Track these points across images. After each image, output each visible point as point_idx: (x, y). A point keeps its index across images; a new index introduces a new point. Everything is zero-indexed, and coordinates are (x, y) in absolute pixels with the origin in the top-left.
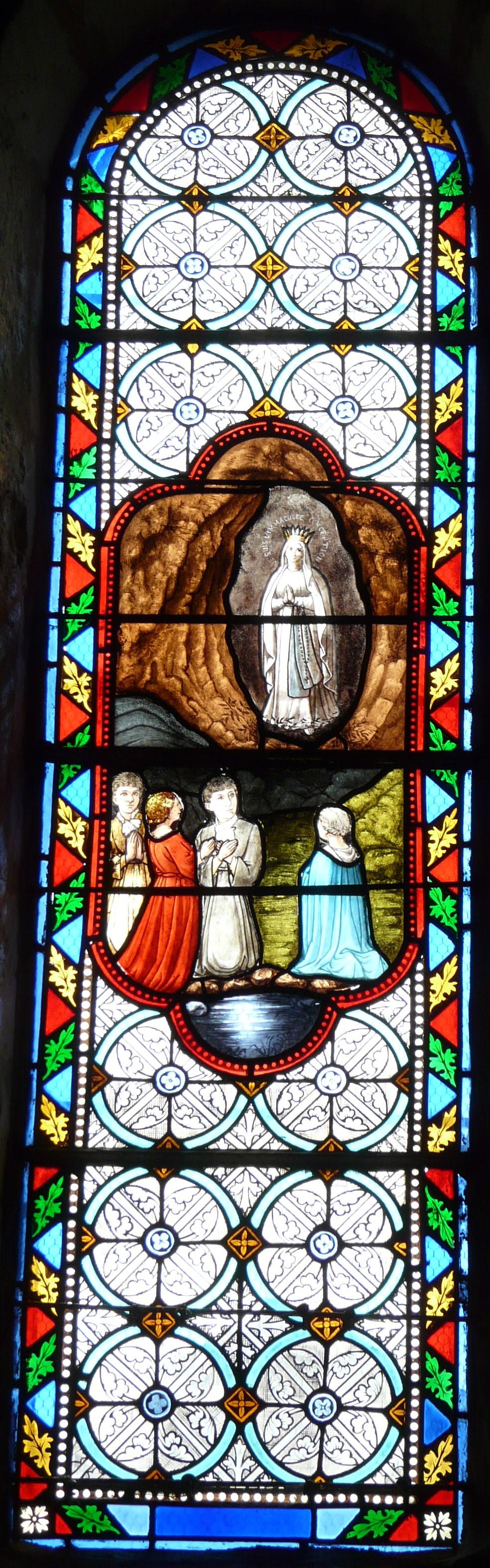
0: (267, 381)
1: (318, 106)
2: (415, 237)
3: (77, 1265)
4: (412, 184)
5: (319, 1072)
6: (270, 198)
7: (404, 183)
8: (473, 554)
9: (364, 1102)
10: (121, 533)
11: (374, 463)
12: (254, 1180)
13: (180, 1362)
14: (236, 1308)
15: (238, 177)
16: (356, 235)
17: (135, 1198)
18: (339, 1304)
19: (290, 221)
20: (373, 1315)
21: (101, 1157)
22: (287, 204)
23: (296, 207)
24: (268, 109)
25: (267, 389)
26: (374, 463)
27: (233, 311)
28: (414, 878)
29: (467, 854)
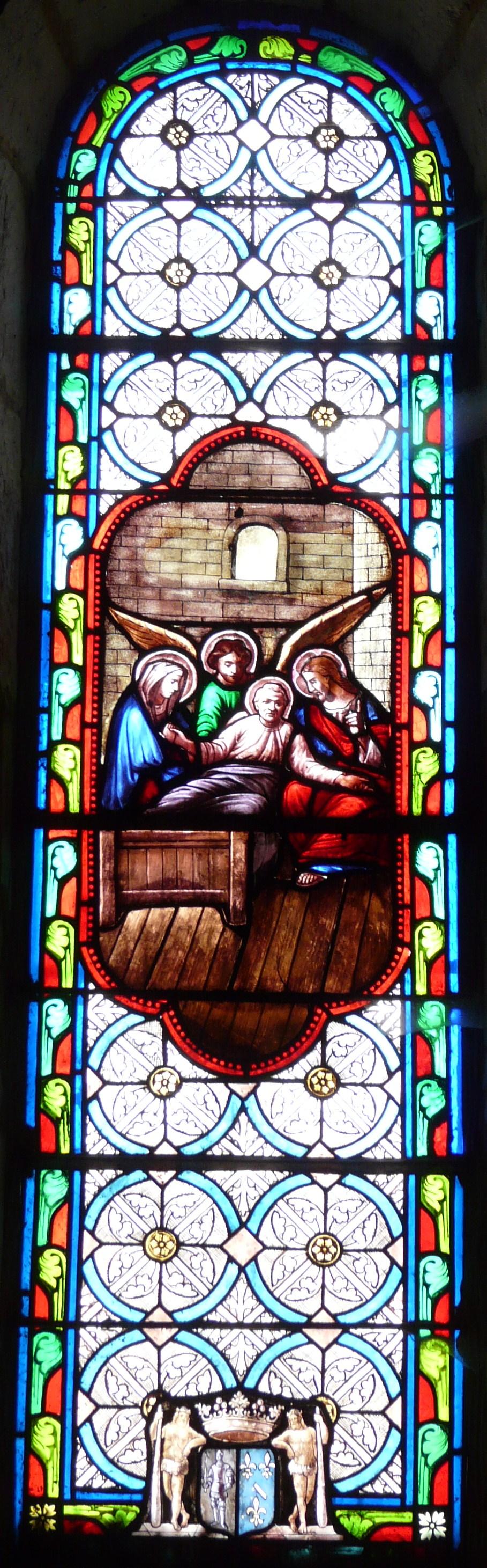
0: (242, 1284)
1: (296, 104)
2: (398, 1212)
3: (99, 439)
4: (393, 188)
5: (310, 1240)
6: (240, 1325)
7: (384, 1475)
8: (456, 612)
9: (355, 1273)
10: (111, 539)
11: (356, 1308)
12: (252, 1184)
13: (185, 1207)
14: (248, 194)
15: (219, 318)
16: (336, 384)
17: (134, 1204)
18: (340, 188)
19: (262, 1352)
20: (367, 199)
21: (116, 344)
22: (259, 1332)
23: (268, 1335)
24: (234, 1372)
25: (241, 1379)
26: (356, 1308)
27: (216, 321)
28: (402, 899)
29: (457, 1461)
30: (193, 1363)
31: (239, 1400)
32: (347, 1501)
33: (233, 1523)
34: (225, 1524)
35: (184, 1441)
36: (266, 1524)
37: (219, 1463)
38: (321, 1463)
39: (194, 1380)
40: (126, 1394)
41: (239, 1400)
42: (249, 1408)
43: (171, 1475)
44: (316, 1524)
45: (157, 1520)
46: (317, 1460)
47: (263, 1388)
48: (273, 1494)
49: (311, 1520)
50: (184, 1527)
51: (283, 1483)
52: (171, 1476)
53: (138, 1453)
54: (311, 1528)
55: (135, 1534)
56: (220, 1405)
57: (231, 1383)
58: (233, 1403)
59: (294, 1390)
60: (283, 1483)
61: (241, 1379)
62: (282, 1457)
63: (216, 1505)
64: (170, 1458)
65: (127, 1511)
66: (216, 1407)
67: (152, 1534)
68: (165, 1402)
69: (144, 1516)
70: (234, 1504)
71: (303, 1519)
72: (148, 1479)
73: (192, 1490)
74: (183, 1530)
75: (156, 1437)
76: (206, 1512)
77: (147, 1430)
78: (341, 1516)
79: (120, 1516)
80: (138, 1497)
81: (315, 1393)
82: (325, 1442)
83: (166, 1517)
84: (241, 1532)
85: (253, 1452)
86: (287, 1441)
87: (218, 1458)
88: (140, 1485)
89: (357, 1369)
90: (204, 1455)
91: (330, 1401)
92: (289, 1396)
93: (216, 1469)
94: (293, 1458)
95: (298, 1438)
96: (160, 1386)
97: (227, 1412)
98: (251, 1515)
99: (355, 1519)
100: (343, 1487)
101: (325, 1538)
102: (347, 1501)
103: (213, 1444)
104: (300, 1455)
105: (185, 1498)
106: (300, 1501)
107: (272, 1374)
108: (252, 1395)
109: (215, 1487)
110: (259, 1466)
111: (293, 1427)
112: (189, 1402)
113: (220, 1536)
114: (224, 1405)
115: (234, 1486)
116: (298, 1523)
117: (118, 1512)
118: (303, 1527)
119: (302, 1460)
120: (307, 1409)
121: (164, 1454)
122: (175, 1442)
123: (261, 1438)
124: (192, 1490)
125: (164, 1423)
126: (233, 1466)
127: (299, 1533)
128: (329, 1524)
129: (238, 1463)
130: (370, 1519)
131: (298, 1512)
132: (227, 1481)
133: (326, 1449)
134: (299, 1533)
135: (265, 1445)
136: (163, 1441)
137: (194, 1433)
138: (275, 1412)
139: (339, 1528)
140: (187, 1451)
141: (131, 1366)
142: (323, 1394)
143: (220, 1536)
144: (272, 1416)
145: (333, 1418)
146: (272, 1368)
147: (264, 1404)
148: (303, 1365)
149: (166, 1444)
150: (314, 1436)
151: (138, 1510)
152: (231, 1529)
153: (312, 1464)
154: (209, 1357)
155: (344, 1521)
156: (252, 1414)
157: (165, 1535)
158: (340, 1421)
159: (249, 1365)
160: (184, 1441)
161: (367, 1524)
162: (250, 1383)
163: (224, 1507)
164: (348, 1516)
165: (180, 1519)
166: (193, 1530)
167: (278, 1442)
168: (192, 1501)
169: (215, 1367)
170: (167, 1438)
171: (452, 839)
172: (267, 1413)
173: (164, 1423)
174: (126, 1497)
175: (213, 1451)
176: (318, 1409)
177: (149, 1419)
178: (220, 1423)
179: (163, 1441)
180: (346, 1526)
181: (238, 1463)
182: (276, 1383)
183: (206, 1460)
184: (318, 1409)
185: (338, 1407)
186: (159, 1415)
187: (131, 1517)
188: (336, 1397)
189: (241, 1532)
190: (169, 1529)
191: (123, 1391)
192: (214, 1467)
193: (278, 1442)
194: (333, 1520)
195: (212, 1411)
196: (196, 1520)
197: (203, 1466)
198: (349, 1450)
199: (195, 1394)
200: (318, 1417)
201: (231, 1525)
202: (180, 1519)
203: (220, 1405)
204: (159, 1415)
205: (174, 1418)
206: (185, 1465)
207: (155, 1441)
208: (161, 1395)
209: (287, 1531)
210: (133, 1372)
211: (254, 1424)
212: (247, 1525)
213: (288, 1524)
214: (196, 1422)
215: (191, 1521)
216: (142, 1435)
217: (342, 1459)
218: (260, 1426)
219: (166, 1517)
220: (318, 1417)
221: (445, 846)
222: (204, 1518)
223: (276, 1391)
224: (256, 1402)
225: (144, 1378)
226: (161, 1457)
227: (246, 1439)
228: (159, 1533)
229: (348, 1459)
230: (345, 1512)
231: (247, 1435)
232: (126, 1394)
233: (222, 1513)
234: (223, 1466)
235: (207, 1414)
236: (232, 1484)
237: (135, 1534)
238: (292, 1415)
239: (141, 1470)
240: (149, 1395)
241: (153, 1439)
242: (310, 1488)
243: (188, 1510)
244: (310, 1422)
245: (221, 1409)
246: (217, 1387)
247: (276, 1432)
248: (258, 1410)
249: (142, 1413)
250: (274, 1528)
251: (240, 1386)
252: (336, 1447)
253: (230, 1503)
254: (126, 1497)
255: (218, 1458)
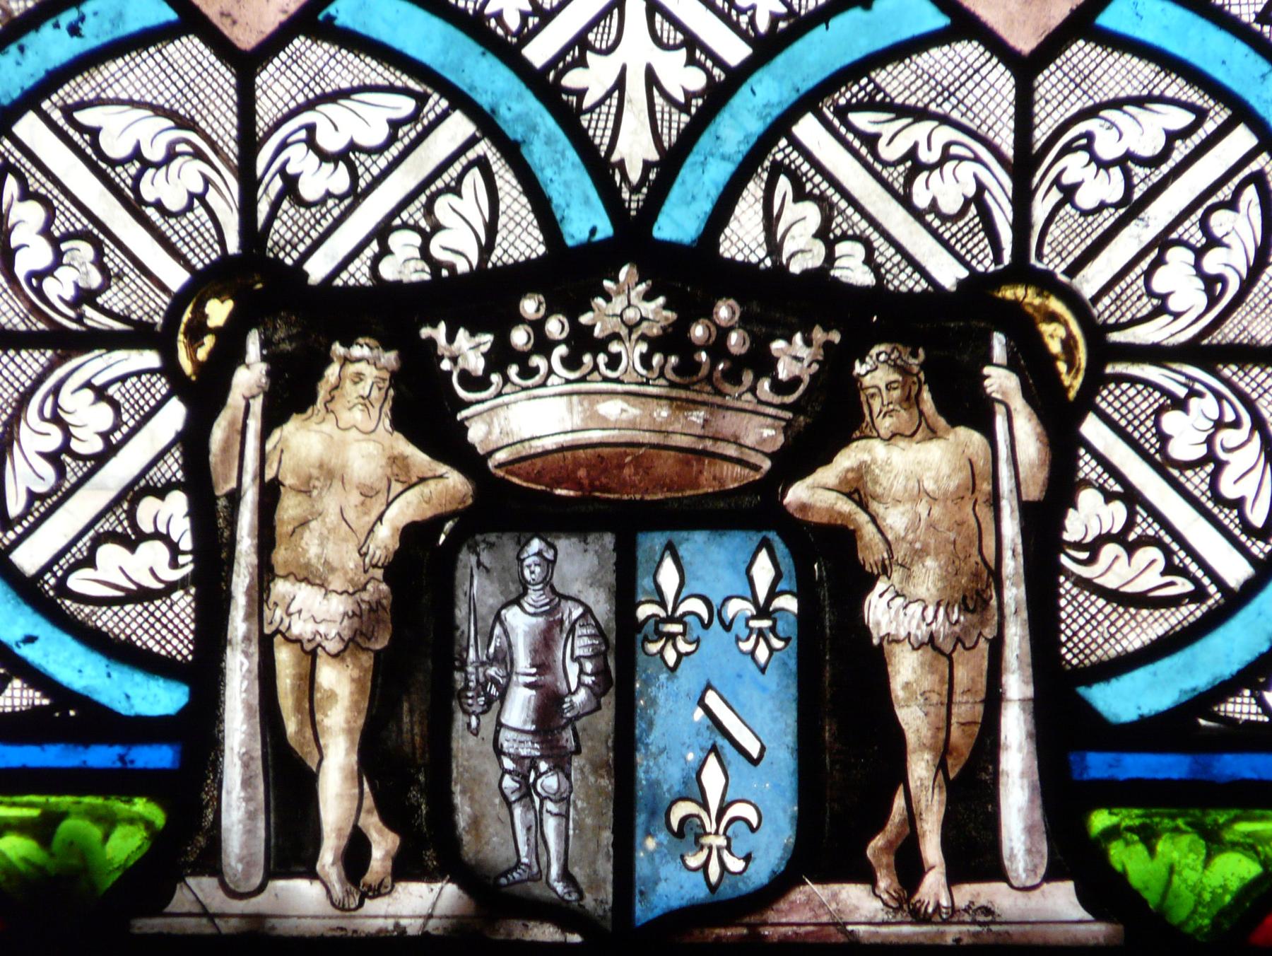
24: (601, 167)
25: (633, 202)
30: (408, 133)
31: (628, 304)
32: (1138, 765)
33: (606, 868)
34: (566, 876)
35: (368, 493)
36: (760, 874)
37: (535, 597)
38: (1014, 593)
39: (414, 213)
40: (95, 279)
41: (628, 304)
42: (671, 341)
43: (310, 654)
44: (995, 871)
45: (248, 862)
46: (996, 575)
47: (743, 239)
48: (790, 739)
49: (975, 853)
50: (377, 891)
51: (838, 682)
52: (313, 654)
53: (154, 553)
54: (966, 893)
55: (149, 925)
56: (538, 326)
57: (585, 220)
58: (601, 317)
59: (885, 252)
60: (838, 682)
61: (633, 202)
62: (832, 568)
63: (527, 791)
64: (307, 576)
65: (108, 822)
66: (520, 337)
67: (227, 927)
68: (275, 313)
69: (188, 838)
70: (607, 783)
71: (932, 850)
72: (202, 673)
73: (410, 723)
74: (371, 906)
75: (237, 475)
76: (475, 822)
77: (193, 441)
78: (1113, 833)
79: (77, 848)
80: (158, 757)
81: (986, 265)
82: (1033, 492)
83: (292, 846)
84: (643, 913)
85: (695, 544)
86: (857, 490)
87: (533, 571)
88: (161, 698)
89: (1182, 150)
90: (466, 559)
91: (1056, 305)
92: (864, 277)
93: (521, 624)
94: (885, 570)
95: (905, 470)
96: (253, 234)
97: (571, 362)
98: (689, 833)
99: (1180, 849)
100: (1121, 700)
101: (1037, 935)
102: (1138, 765)
103: (513, 504)
104: (920, 554)
105: (377, 760)
106: (920, 768)
107: (784, 184)
108: (691, 275)
109: (519, 708)
110: (721, 587)
111: (885, 425)
112: (390, 313)
113: (546, 933)
114: (555, 327)
115: (609, 701)
116: (909, 867)
117: (68, 826)
118: (933, 887)
119: (928, 579)
120: (949, 340)
121: (280, 555)
122: (331, 502)
123: (734, 476)
124: (410, 723)
125: (274, 418)
126: (602, 607)
127: (919, 916)
128: (1053, 874)
129: (625, 595)
130: (1249, 847)
131: (912, 817)
132: (575, 676)
133: (1044, 521)
134: (919, 916)
135: (753, 509)
136: (270, 493)
137: (419, 458)
138: (794, 357)
139: (1103, 888)
140: (385, 538)
141: (115, 146)
142: (1021, 271)
143: (546, 933)
144: (783, 373)
145: (1073, 383)
146: (781, 150)
147: (745, 322)
148: (927, 138)
149: (289, 508)
150: (982, 464)
151: (158, 816)
152: (598, 899)
153: (975, 594)
154: (484, 100)
155: (1128, 858)
156: (688, 368)
157: (286, 927)
158: (1106, 399)
159: (670, 137)
160: (368, 493)
161: (1235, 870)
162: (678, 222)
163: (563, 799)
164: (1148, 836)
165: (356, 852)
166: (417, 903)
167: (812, 493)
168: (407, 770)
169: (512, 152)
170: (289, 480)
171: (459, 417)
172: (763, 363)
173: (272, 420)
174: (102, 756)
175: (508, 544)
176: (999, 343)
177: (204, 394)
178: (529, 419)
179: (270, 493)
180: (1135, 879)
181: (625, 595)
182: (800, 223)
183: (477, 586)
184: (999, 343)
185: (1095, 331)
186: (249, 377)
187: (124, 845)
188: (1089, 282)
189: (643, 913)
190: (304, 900)
191: (79, 269)
192: (513, 615)
193: (812, 493)
194: (1072, 854)
195: (500, 357)
196: (430, 858)
197: (461, 612)
198: (1145, 526)
199: (416, 273)
200: (1000, 381)
201: (596, 885)
202: (356, 852)
203: (538, 326)
204: (249, 377)
205: (323, 391)
206: (375, 608)
207: (235, 497)
208: (256, 279)
209: (860, 905)
210: (123, 176)
211: (698, 416)
212: (672, 882)
213: (866, 876)
214: (424, 408)
215: (407, 867)
216: (172, 468)
217: (1115, 569)
218: (729, 423)
219: (292, 846)
220: (1000, 381)
221: (467, 418)
222: (469, 847)
223: (802, 252)
224: (707, 312)
225: (175, 202)
226: (265, 573)
227: (661, 484)
228: (259, 918)
229: (1141, 571)
230: (1129, 817)
231: (666, 465)
232: (95, 279)
233: (551, 826)
234: (551, 611)
235: (477, 364)
236: (597, 692)
237: (149, 925)
238: (875, 373)
239: (171, 627)
240: (204, 283)
241: (223, 487)
242: (967, 709)
243: (392, 817)
244: (971, 409)
245: (543, 345)
246: (522, 241)
247: (802, 455)
248: (718, 347)
249: (170, 368)
250: (798, 895)
251: (632, 239)
252: (1090, 515)
253: (588, 779)
254: (102, 756)
255: (533, 571)
